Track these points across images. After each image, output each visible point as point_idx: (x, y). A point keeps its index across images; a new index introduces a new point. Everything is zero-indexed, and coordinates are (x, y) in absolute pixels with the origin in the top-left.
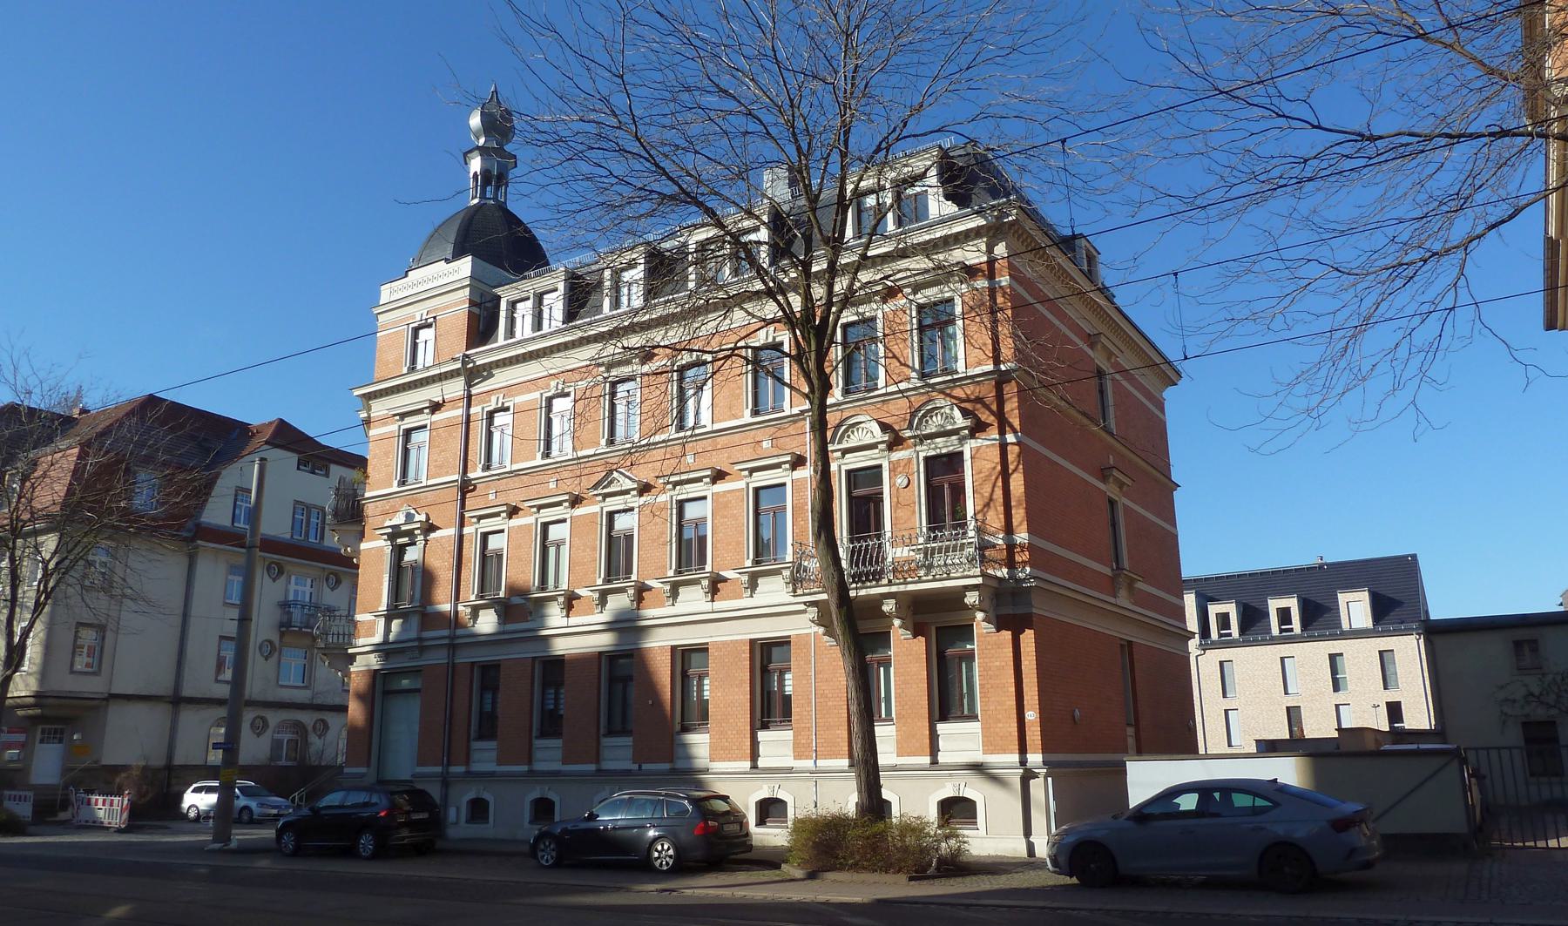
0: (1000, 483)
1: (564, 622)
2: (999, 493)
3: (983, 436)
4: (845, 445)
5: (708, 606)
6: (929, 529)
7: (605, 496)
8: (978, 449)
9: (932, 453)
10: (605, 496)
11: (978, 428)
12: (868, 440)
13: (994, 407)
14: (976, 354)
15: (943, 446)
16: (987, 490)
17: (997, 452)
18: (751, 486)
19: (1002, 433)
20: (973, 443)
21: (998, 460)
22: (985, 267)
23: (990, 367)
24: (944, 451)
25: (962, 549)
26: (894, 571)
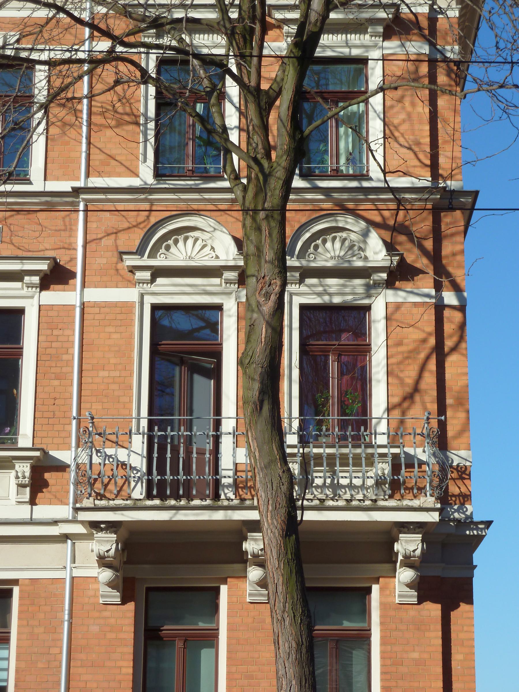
0: (432, 365)
1: (24, 512)
2: (429, 380)
3: (409, 286)
4: (159, 262)
5: (24, 512)
6: (151, 424)
7: (158, 273)
8: (398, 306)
9: (316, 300)
10: (158, 273)
11: (400, 273)
12: (205, 260)
13: (429, 244)
14: (401, 156)
15: (337, 292)
16: (410, 374)
17: (430, 316)
18: (149, 300)
19: (438, 287)
20: (390, 296)
21: (431, 328)
22: (424, 23)
23: (425, 182)
24: (337, 300)
25: (370, 463)
26: (236, 485)
